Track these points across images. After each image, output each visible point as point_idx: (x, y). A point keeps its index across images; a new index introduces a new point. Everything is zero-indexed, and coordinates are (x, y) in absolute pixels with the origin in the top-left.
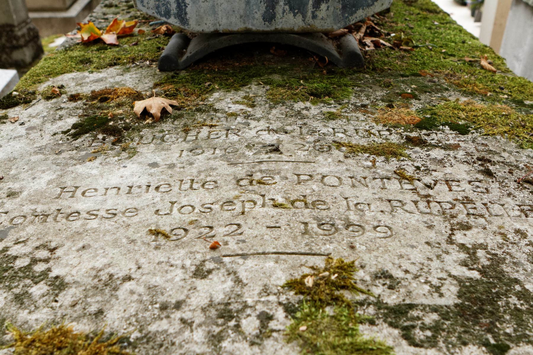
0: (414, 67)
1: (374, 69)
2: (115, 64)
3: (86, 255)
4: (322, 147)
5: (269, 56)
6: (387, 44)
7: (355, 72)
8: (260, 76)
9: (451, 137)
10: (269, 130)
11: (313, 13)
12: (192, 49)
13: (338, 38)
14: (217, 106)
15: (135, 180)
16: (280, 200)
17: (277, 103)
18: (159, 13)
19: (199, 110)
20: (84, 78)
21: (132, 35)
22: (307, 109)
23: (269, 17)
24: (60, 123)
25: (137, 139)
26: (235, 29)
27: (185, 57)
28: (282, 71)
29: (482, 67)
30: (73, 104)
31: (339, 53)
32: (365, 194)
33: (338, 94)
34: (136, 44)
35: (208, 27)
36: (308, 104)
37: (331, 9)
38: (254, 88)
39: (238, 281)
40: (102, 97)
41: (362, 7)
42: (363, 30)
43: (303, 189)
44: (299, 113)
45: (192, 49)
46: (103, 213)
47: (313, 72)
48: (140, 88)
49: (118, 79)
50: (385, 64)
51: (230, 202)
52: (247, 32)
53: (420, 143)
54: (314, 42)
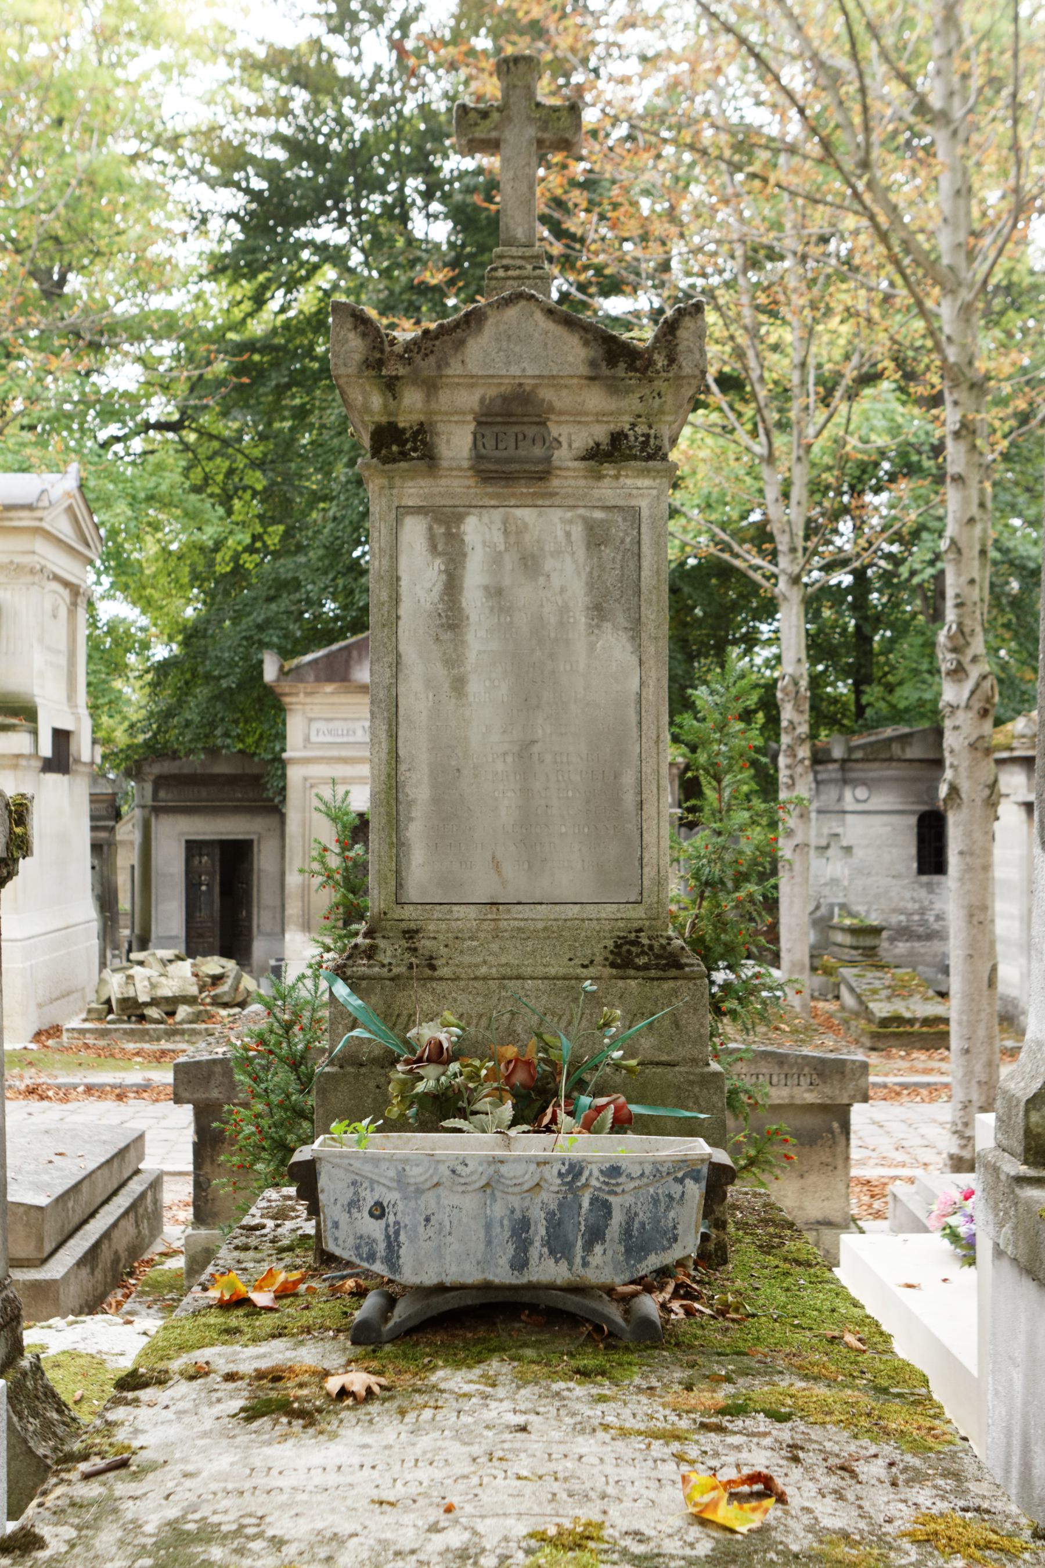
0: (741, 1344)
1: (677, 1345)
2: (280, 1335)
3: (301, 1521)
4: (583, 1428)
5: (517, 1325)
6: (708, 1311)
7: (647, 1348)
8: (504, 1350)
9: (762, 1423)
10: (515, 1412)
11: (583, 1258)
12: (401, 1311)
13: (626, 1300)
14: (442, 1386)
15: (343, 1460)
16: (524, 1473)
17: (527, 1383)
18: (359, 1256)
19: (418, 1391)
20: (235, 1353)
21: (296, 1295)
22: (569, 1389)
23: (520, 1263)
24: (220, 1407)
25: (336, 1423)
26: (469, 1280)
27: (391, 1324)
28: (537, 1345)
29: (847, 1345)
30: (231, 1386)
31: (626, 1320)
32: (628, 1473)
33: (617, 1373)
34: (307, 1308)
35: (429, 1278)
36: (571, 1385)
37: (610, 1253)
38: (495, 1365)
39: (475, 1533)
40: (276, 1376)
41: (655, 1250)
42: (670, 1288)
43: (552, 1466)
44: (558, 1394)
45: (401, 1311)
46: (309, 1488)
47: (582, 1345)
48: (327, 1365)
49: (289, 1354)
50: (696, 1338)
51: (466, 1477)
52: (487, 1287)
53: (720, 1429)
54: (586, 1302)
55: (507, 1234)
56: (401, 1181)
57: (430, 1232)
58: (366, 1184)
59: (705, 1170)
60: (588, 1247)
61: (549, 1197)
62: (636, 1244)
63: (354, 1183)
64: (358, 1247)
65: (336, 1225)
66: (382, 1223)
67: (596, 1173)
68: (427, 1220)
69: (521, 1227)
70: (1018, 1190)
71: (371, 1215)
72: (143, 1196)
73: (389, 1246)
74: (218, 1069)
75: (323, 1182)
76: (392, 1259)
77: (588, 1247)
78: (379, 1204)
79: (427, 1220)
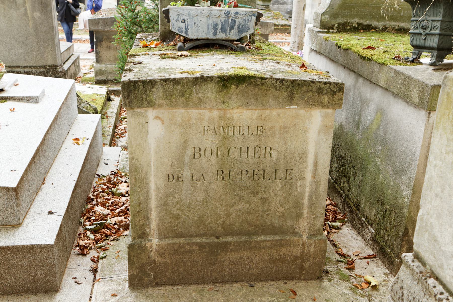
23: (215, 34)
52: (207, 39)
55: (212, 27)
56: (189, 14)
57: (195, 26)
58: (181, 15)
59: (256, 14)
60: (230, 31)
61: (222, 19)
62: (241, 30)
63: (178, 15)
64: (179, 30)
65: (174, 25)
66: (184, 24)
67: (233, 13)
68: (195, 23)
69: (216, 25)
70: (318, 34)
71: (182, 22)
72: (75, 60)
73: (186, 29)
74: (101, 21)
75: (171, 14)
76: (187, 32)
77: (230, 31)
78: (184, 20)
79: (195, 23)
